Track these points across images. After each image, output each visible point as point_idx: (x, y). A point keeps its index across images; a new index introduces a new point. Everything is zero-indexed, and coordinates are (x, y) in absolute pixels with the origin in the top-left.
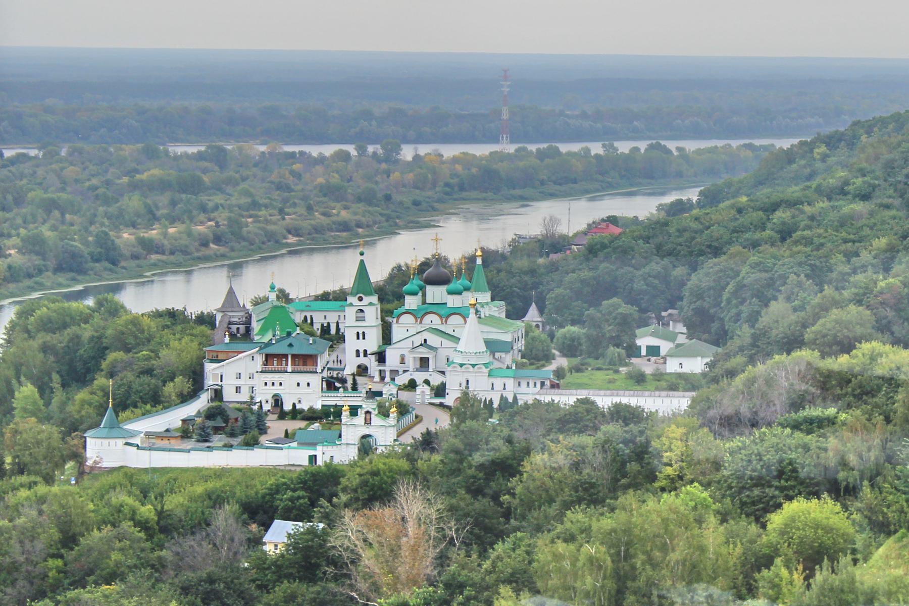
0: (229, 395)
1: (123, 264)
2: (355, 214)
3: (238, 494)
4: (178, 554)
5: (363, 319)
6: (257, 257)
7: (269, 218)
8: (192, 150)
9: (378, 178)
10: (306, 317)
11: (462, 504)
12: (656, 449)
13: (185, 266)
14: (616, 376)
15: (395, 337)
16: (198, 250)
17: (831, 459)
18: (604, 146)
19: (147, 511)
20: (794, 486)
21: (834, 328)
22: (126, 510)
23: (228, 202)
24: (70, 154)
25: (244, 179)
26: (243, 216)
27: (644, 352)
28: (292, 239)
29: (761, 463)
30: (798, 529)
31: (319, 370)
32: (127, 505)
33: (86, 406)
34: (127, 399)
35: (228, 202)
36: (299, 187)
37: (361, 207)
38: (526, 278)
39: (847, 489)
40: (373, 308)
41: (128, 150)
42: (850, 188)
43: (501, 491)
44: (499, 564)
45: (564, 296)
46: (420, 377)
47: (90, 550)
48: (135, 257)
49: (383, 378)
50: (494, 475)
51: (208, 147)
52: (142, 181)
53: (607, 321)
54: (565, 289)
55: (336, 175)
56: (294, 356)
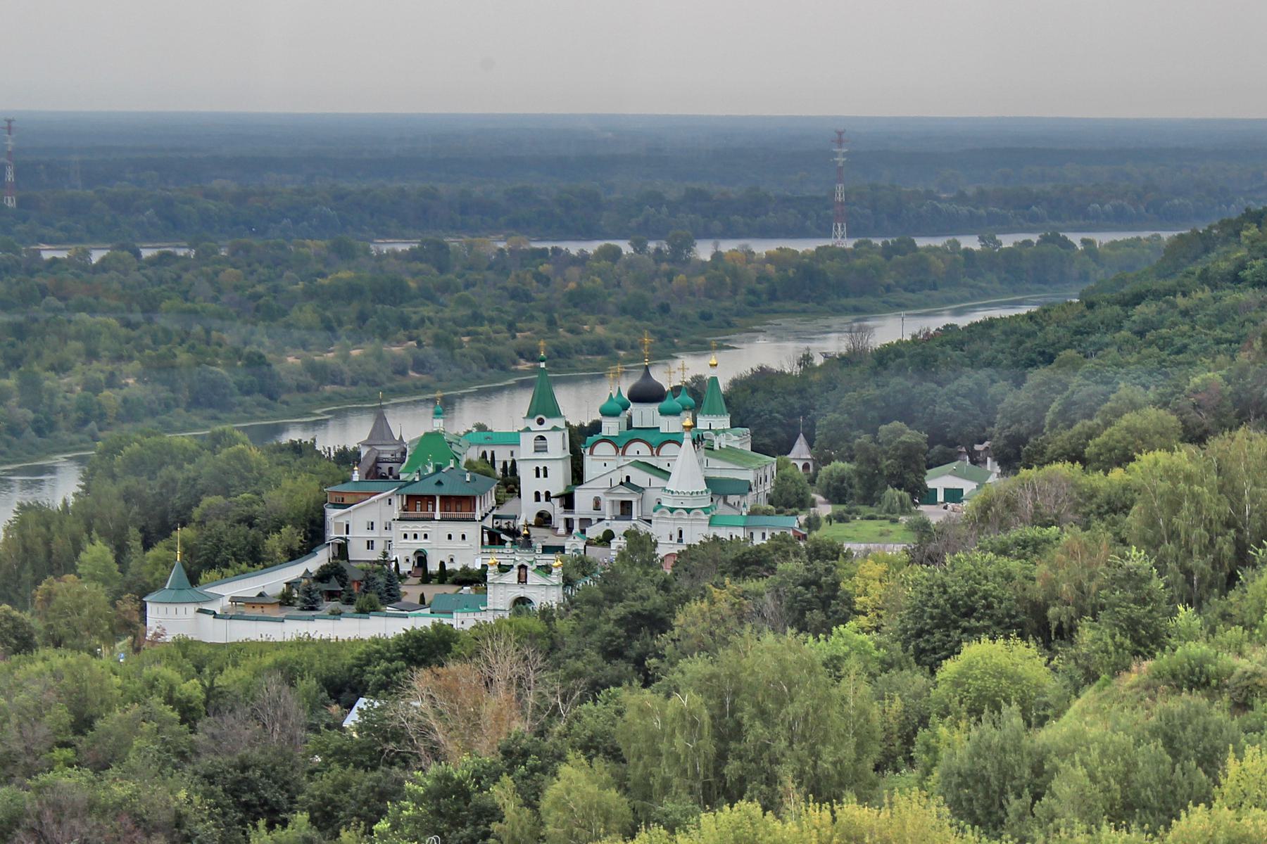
0: (358, 552)
1: (285, 397)
2: (616, 330)
3: (317, 665)
4: (213, 737)
5: (543, 449)
6: (473, 389)
7: (493, 335)
8: (402, 247)
9: (656, 283)
10: (484, 454)
11: (590, 668)
12: (846, 593)
13: (371, 401)
14: (892, 527)
15: (588, 475)
16: (391, 380)
17: (1037, 591)
18: (981, 239)
19: (192, 688)
20: (988, 627)
21: (1124, 439)
22: (162, 685)
23: (440, 315)
24: (234, 253)
25: (468, 286)
26: (456, 334)
27: (940, 498)
28: (524, 365)
29: (945, 597)
30: (976, 679)
31: (478, 517)
32: (163, 678)
33: (161, 566)
34: (216, 556)
35: (440, 315)
36: (543, 296)
37: (626, 321)
38: (792, 400)
39: (1060, 631)
40: (559, 434)
41: (315, 246)
42: (1247, 273)
43: (647, 654)
44: (576, 725)
45: (840, 423)
46: (620, 527)
47: (109, 734)
48: (302, 388)
49: (569, 529)
50: (639, 632)
51: (423, 243)
52: (322, 286)
53: (886, 452)
54: (841, 413)
55: (598, 280)
56: (445, 499)
